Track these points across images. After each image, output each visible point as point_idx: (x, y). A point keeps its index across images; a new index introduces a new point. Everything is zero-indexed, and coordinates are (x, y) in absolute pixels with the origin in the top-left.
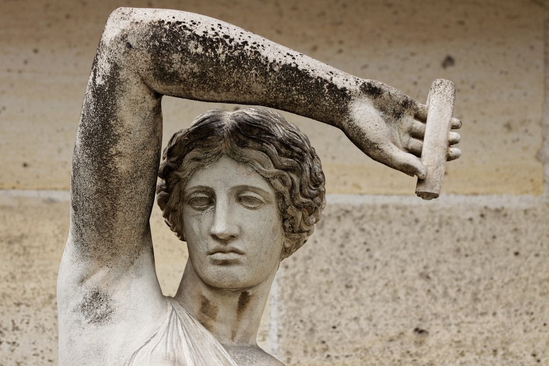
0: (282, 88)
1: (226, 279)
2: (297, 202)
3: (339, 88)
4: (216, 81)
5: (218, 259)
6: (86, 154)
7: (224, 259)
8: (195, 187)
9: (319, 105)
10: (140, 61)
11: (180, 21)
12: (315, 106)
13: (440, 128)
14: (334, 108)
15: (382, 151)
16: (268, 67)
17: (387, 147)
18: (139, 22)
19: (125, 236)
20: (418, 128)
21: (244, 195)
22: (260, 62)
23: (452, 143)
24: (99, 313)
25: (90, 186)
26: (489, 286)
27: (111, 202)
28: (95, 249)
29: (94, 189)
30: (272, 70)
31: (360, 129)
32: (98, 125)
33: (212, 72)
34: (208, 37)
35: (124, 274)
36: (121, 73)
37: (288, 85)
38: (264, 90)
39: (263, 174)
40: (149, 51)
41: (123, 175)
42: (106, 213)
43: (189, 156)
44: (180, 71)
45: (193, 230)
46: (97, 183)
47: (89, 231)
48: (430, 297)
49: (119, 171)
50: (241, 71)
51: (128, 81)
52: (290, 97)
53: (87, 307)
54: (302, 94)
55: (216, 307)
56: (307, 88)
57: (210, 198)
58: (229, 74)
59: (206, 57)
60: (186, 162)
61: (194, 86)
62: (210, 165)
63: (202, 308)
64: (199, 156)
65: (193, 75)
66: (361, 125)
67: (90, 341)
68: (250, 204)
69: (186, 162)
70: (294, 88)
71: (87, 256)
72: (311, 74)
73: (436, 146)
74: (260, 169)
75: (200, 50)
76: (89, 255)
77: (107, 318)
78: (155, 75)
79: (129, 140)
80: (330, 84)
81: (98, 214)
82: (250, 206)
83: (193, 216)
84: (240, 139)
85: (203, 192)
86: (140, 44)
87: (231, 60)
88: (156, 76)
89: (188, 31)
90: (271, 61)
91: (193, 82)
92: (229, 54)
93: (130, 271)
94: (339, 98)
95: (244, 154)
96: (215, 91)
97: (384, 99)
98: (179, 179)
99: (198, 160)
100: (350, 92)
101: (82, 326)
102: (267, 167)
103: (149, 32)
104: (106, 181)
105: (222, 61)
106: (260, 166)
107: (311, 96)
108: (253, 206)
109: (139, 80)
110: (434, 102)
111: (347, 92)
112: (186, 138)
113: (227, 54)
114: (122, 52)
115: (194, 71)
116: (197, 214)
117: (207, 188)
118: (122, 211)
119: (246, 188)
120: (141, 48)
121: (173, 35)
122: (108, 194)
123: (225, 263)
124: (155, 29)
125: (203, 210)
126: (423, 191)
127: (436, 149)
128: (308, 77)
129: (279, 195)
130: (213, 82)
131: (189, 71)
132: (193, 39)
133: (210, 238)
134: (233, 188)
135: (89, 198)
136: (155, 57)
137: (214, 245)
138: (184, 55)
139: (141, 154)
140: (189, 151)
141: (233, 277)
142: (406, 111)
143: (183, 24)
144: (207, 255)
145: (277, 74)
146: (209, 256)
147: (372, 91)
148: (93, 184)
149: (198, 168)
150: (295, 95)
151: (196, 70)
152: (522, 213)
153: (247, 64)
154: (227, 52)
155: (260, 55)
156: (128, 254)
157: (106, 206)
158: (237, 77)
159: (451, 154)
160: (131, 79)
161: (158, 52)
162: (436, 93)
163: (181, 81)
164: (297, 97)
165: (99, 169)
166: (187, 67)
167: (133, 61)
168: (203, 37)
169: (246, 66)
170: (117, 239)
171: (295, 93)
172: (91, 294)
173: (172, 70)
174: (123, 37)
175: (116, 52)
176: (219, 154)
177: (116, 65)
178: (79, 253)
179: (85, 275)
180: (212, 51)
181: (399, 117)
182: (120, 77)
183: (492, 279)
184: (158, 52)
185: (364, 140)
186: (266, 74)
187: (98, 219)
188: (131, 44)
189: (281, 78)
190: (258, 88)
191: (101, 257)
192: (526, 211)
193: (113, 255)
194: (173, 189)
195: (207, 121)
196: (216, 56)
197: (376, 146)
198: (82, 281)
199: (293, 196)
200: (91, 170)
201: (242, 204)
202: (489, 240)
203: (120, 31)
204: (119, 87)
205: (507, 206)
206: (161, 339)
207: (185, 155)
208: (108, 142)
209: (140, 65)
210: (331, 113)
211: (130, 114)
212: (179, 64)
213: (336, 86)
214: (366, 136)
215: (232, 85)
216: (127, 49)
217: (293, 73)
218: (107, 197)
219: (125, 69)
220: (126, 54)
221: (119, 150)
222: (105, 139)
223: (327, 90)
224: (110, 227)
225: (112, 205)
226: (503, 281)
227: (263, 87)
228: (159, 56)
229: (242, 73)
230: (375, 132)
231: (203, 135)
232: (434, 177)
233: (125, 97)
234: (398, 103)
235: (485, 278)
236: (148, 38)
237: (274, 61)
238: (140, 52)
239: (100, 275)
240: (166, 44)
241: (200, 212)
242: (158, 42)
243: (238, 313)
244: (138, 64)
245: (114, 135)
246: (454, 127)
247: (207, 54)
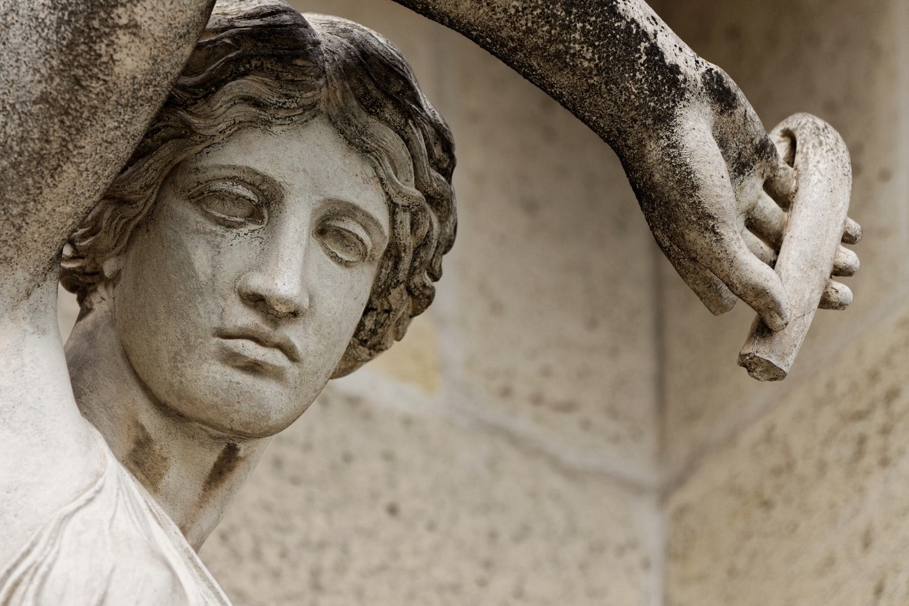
0: (555, 16)
1: (245, 406)
2: (417, 280)
3: (667, 61)
5: (246, 353)
8: (234, 168)
9: (615, 84)
12: (606, 84)
13: (827, 231)
14: (646, 103)
15: (719, 239)
19: (51, 227)
23: (839, 272)
25: (29, 78)
27: (66, 136)
29: (37, 91)
31: (689, 173)
35: (6, 315)
37: (569, 13)
39: (392, 191)
41: (121, 83)
42: (42, 157)
43: (236, 87)
45: (191, 264)
46: (52, 79)
49: (117, 70)
54: (592, 45)
56: (606, 36)
57: (263, 204)
60: (225, 98)
62: (285, 127)
63: (134, 451)
66: (694, 166)
69: (225, 98)
70: (579, 25)
73: (812, 267)
74: (389, 178)
80: (652, 44)
81: (20, 154)
82: (340, 255)
83: (198, 231)
84: (367, 92)
85: (251, 185)
93: (20, 313)
94: (663, 85)
95: (370, 131)
97: (734, 122)
98: (187, 133)
99: (257, 103)
100: (685, 80)
102: (403, 179)
104: (77, 80)
106: (391, 171)
107: (608, 56)
108: (346, 257)
110: (821, 166)
111: (681, 77)
112: (228, 41)
116: (211, 232)
117: (265, 179)
119: (351, 211)
122: (67, 113)
123: (254, 368)
125: (229, 226)
126: (765, 357)
127: (812, 274)
129: (393, 253)
133: (234, 299)
134: (329, 201)
135: (13, 106)
141: (261, 406)
142: (758, 165)
144: (214, 335)
146: (216, 340)
148: (38, 77)
149: (252, 123)
150: (575, 41)
156: (32, 270)
157: (48, 141)
159: (834, 297)
162: (825, 148)
164: (578, 47)
165: (72, 45)
171: (577, 37)
176: (311, 109)
181: (741, 173)
187: (14, 165)
197: (711, 223)
199: (417, 264)
200: (48, 41)
201: (323, 244)
206: (117, 503)
207: (225, 82)
213: (662, 55)
214: (700, 193)
218: (62, 122)
221: (138, 18)
223: (644, 58)
225: (64, 144)
230: (719, 190)
232: (793, 335)
234: (752, 139)
241: (219, 229)
243: (204, 490)
246: (848, 239)
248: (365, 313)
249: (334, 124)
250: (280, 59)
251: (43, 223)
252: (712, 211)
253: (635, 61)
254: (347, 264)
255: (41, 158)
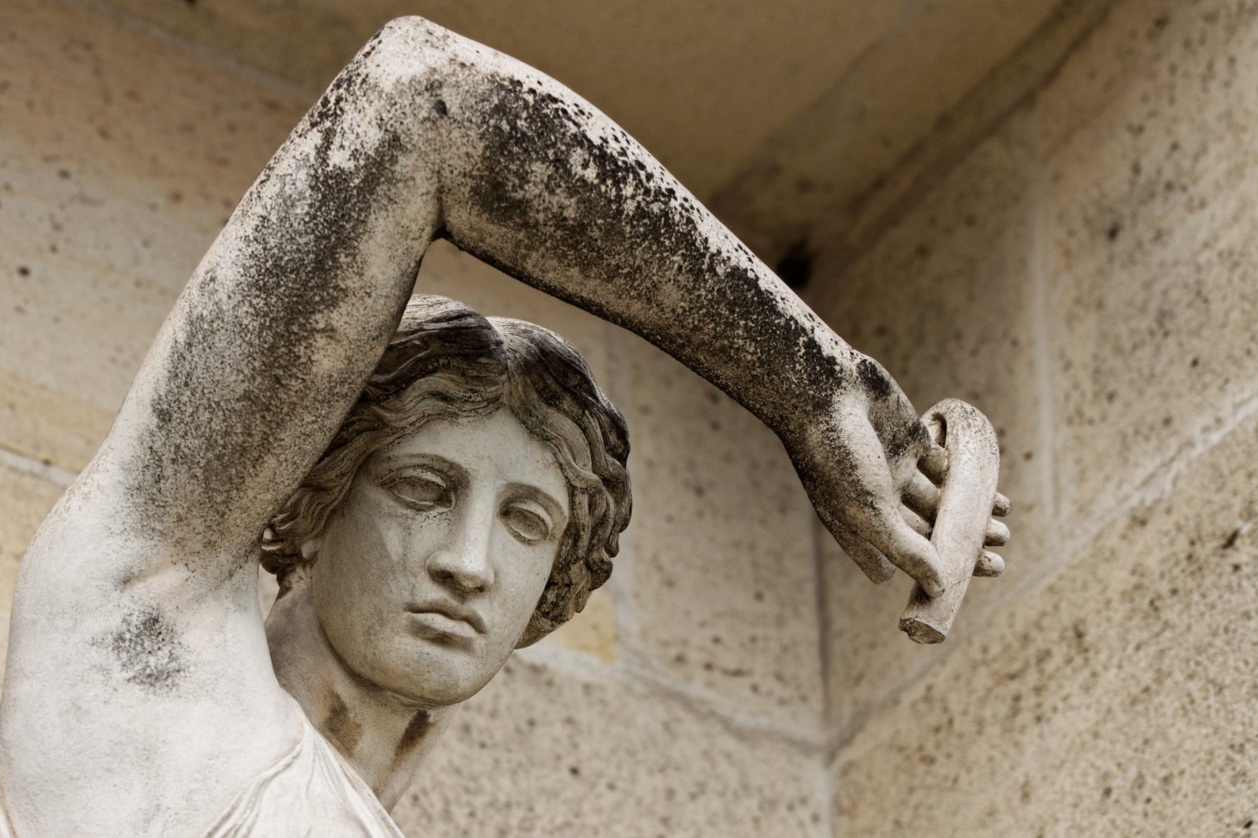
0: (720, 315)
1: (434, 676)
2: (595, 556)
3: (824, 354)
4: (598, 252)
5: (435, 626)
6: (251, 304)
7: (447, 630)
8: (424, 456)
9: (777, 374)
10: (454, 148)
11: (555, 95)
12: (769, 375)
15: (878, 514)
16: (707, 260)
17: (889, 509)
18: (468, 64)
20: (921, 488)
21: (524, 507)
22: (693, 244)
24: (152, 664)
25: (233, 378)
26: (527, 824)
28: (180, 519)
30: (712, 269)
31: (848, 454)
32: (308, 253)
33: (600, 229)
34: (609, 151)
36: (402, 159)
37: (732, 312)
38: (682, 304)
39: (571, 475)
40: (482, 136)
43: (425, 384)
44: (535, 203)
46: (254, 379)
47: (183, 477)
48: (418, 811)
50: (654, 248)
51: (411, 183)
52: (727, 337)
53: (127, 643)
54: (755, 340)
55: (359, 726)
57: (449, 489)
58: (631, 247)
59: (599, 193)
60: (415, 394)
61: (548, 244)
63: (330, 719)
64: (452, 391)
65: (560, 221)
66: (852, 447)
67: (129, 723)
68: (525, 531)
69: (415, 394)
71: (153, 530)
72: (780, 305)
74: (569, 463)
75: (591, 174)
76: (159, 527)
77: (169, 681)
78: (475, 191)
79: (361, 309)
81: (224, 447)
84: (547, 386)
85: (438, 472)
86: (468, 114)
87: (644, 217)
88: (477, 193)
89: (570, 124)
90: (713, 250)
91: (551, 235)
92: (643, 204)
93: (223, 593)
96: (581, 271)
98: (379, 426)
99: (445, 398)
101: (113, 683)
102: (581, 464)
103: (490, 95)
104: (278, 380)
105: (628, 215)
106: (570, 457)
108: (528, 537)
109: (433, 189)
110: (970, 446)
113: (639, 203)
114: (421, 116)
115: (566, 214)
116: (403, 514)
117: (452, 465)
118: (278, 456)
119: (533, 493)
120: (466, 124)
121: (542, 122)
122: (268, 410)
123: (443, 640)
124: (503, 93)
125: (419, 509)
126: (924, 621)
127: (965, 545)
128: (773, 309)
129: (573, 531)
130: (593, 250)
131: (555, 209)
132: (581, 145)
134: (512, 485)
135: (218, 404)
136: (493, 153)
137: (433, 593)
138: (557, 171)
139: (368, 347)
140: (425, 373)
141: (449, 675)
143: (560, 105)
144: (405, 610)
145: (720, 281)
147: (876, 386)
149: (440, 416)
151: (570, 213)
152: (579, 689)
153: (670, 238)
154: (639, 198)
155: (696, 229)
157: (250, 435)
158: (642, 259)
159: (987, 565)
160: (418, 181)
161: (503, 146)
163: (525, 225)
165: (272, 348)
166: (555, 200)
167: (439, 144)
168: (600, 148)
169: (667, 242)
170: (237, 513)
171: (740, 332)
172: (142, 618)
173: (519, 195)
174: (432, 85)
175: (408, 110)
176: (495, 403)
177: (396, 138)
178: (136, 516)
179: (135, 570)
180: (613, 184)
182: (397, 168)
183: (531, 809)
184: (503, 146)
185: (850, 479)
186: (698, 274)
188: (448, 105)
189: (725, 293)
190: (672, 296)
191: (183, 543)
192: (587, 688)
193: (210, 544)
194: (351, 440)
195: (470, 320)
196: (620, 198)
197: (870, 499)
198: (126, 581)
199: (595, 541)
200: (251, 345)
201: (507, 525)
202: (524, 726)
203: (426, 70)
204: (385, 188)
205: (552, 665)
207: (415, 379)
208: (317, 298)
209: (450, 158)
210: (794, 401)
211: (379, 253)
212: (541, 187)
213: (819, 348)
214: (858, 472)
215: (625, 271)
216: (435, 114)
217: (749, 290)
218: (263, 417)
219: (415, 155)
220: (428, 125)
221: (334, 323)
222: (312, 288)
223: (803, 350)
224: (238, 484)
225: (265, 436)
226: (552, 821)
227: (683, 299)
228: (502, 154)
229: (654, 253)
230: (876, 469)
231: (462, 344)
233: (391, 215)
235: (519, 805)
236: (488, 107)
237: (719, 252)
238: (463, 130)
239: (165, 584)
240: (524, 134)
241: (410, 512)
242: (509, 123)
244: (448, 156)
245: (336, 287)
246: (998, 512)
247: (603, 188)
248: (547, 588)
249: (516, 415)
250: (466, 357)
251: (245, 510)
252: (869, 488)
253: (794, 354)
254: (529, 542)
255: (243, 450)
